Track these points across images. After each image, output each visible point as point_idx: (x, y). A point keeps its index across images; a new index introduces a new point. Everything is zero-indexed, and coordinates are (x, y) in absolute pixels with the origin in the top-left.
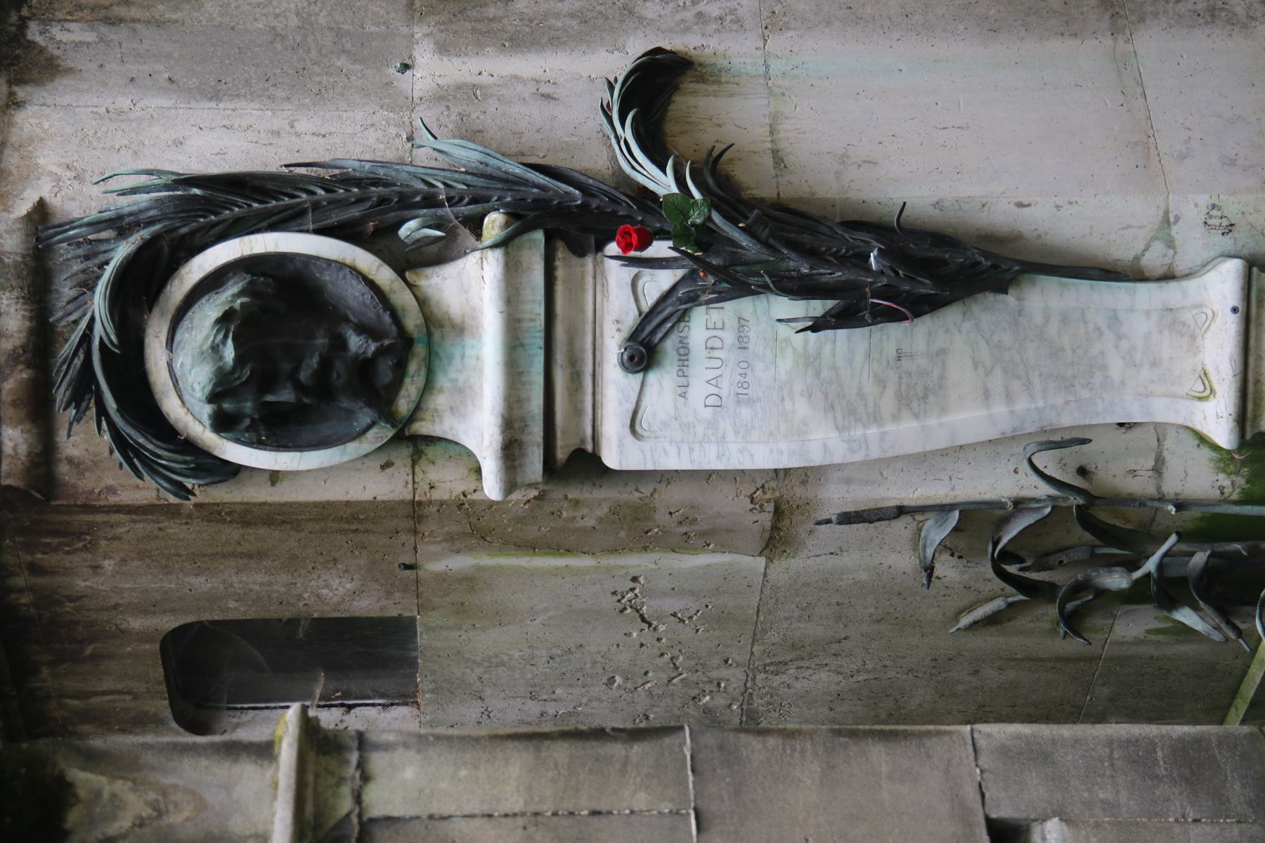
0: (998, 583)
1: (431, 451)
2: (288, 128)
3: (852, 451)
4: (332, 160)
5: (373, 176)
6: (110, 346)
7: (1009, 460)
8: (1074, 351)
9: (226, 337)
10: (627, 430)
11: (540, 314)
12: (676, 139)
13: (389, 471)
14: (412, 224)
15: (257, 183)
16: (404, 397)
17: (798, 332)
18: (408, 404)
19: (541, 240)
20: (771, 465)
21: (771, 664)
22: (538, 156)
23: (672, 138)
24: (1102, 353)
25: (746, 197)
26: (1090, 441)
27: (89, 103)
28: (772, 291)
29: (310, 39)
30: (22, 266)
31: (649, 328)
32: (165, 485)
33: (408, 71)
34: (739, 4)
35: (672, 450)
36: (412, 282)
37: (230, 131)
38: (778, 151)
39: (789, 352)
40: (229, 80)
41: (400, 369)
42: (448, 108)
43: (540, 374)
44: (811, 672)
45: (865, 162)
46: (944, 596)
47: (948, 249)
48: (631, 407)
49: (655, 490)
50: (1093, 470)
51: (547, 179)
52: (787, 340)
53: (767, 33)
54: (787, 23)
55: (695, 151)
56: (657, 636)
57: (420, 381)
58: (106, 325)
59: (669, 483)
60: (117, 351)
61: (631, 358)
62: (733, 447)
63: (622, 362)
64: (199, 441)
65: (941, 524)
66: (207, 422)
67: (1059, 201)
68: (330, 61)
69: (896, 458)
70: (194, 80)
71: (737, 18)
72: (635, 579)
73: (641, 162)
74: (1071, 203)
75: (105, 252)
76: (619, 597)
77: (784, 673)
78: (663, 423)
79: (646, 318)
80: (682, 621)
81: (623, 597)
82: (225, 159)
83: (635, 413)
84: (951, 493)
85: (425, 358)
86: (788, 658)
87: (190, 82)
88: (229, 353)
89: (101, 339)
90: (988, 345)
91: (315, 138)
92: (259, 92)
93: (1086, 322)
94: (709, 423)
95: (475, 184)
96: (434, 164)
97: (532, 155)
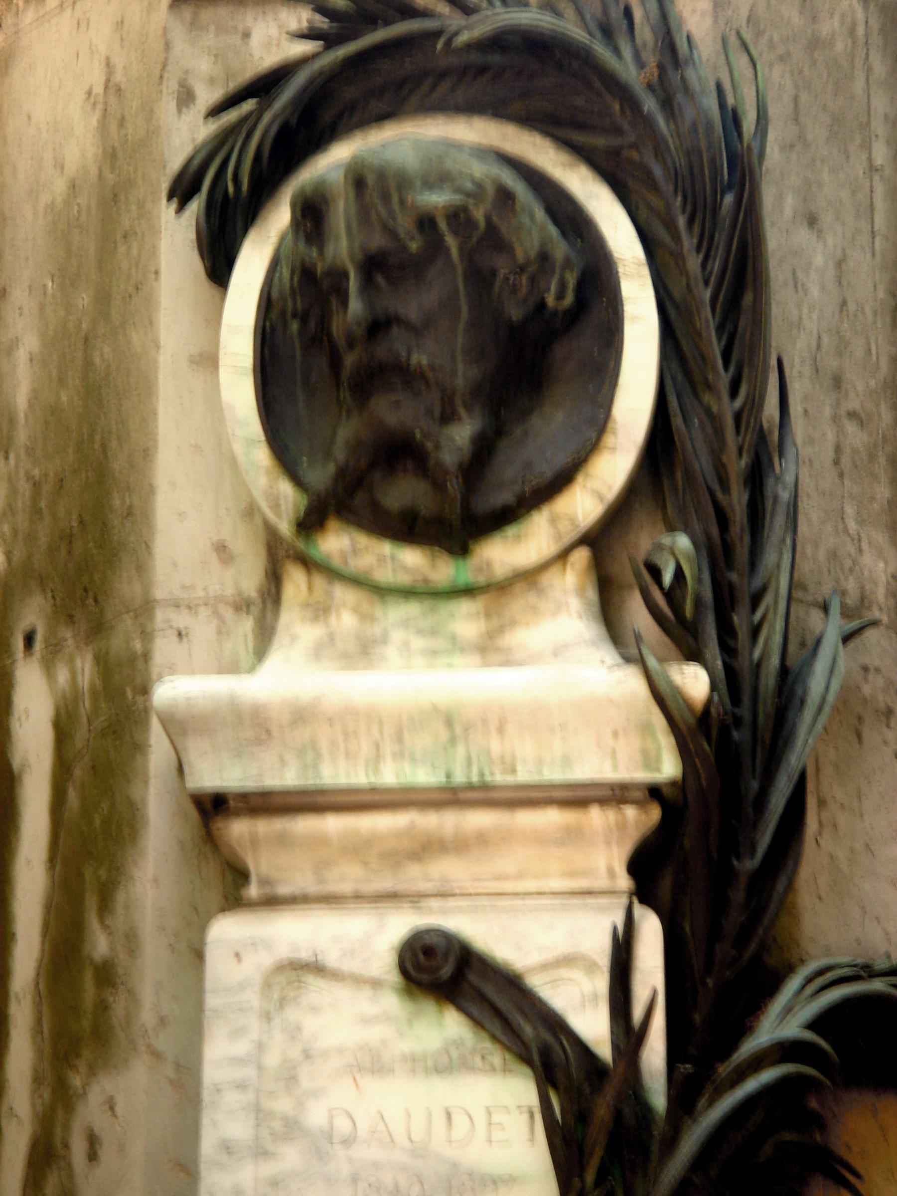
13: (214, 558)
15: (748, 299)
26: (92, 85)
31: (490, 991)
35: (242, 1047)
57: (385, 576)
97: (821, 824)
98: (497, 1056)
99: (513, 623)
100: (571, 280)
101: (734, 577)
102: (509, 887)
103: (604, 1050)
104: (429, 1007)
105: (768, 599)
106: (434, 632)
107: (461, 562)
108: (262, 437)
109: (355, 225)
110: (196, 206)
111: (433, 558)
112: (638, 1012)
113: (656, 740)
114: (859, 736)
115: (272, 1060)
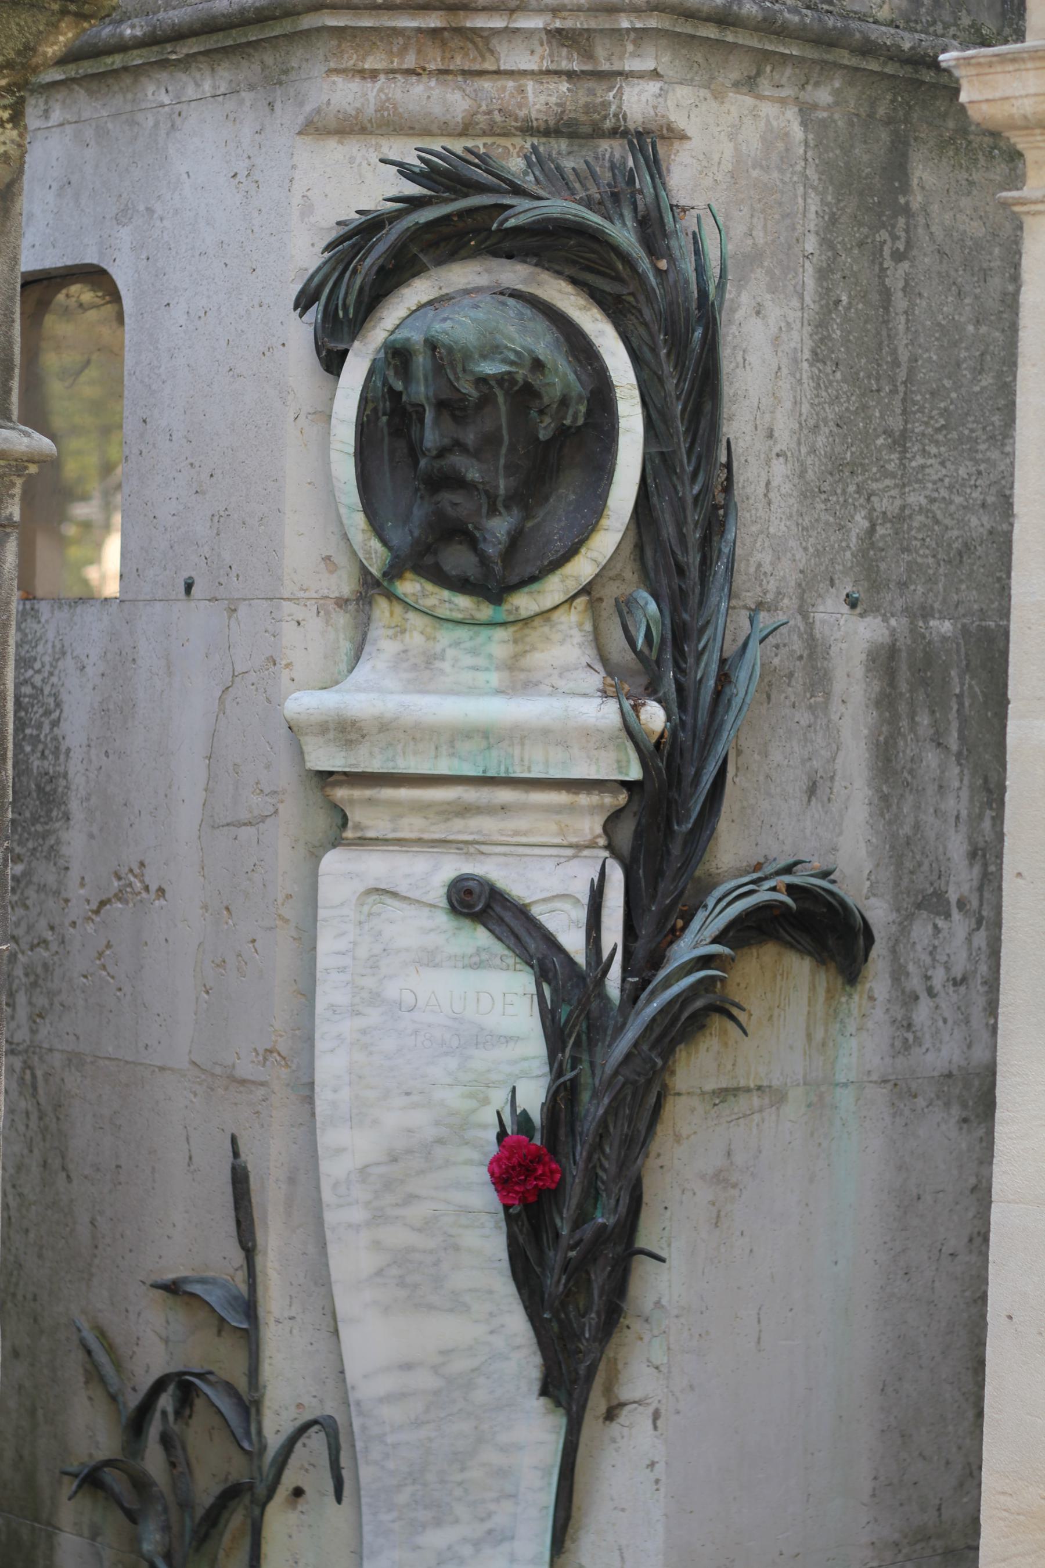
0: (146, 1383)
1: (342, 619)
2: (777, 449)
3: (336, 1185)
4: (735, 504)
5: (715, 558)
6: (501, 217)
7: (315, 1397)
8: (460, 1484)
9: (512, 363)
10: (372, 884)
11: (529, 771)
12: (754, 960)
14: (652, 607)
15: (708, 407)
16: (423, 588)
17: (498, 1113)
18: (414, 595)
19: (627, 775)
20: (319, 1077)
21: (34, 1076)
22: (736, 775)
23: (755, 954)
24: (457, 1521)
25: (677, 1049)
27: (809, 201)
28: (554, 1081)
29: (888, 482)
30: (603, 113)
31: (508, 916)
32: (316, 280)
33: (847, 607)
34: (927, 1050)
35: (342, 944)
36: (574, 604)
37: (773, 375)
38: (735, 1096)
39: (472, 1104)
40: (838, 375)
41: (462, 585)
42: (801, 658)
43: (450, 769)
44: (22, 1128)
45: (719, 1211)
46: (127, 1311)
47: (603, 1317)
48: (403, 890)
49: (287, 921)
50: (300, 1508)
51: (708, 786)
52: (485, 1101)
53: (889, 1086)
54: (901, 1114)
55: (738, 985)
56: (79, 922)
57: (443, 612)
58: (529, 214)
59: (295, 939)
60: (495, 226)
61: (469, 892)
62: (347, 1026)
63: (467, 879)
64: (372, 323)
65: (232, 1305)
66: (402, 334)
67: (660, 1467)
68: (862, 506)
69: (323, 1246)
70: (838, 332)
71: (910, 1047)
72: (161, 891)
73: (728, 910)
74: (657, 1481)
75: (622, 216)
76: (137, 871)
77: (21, 1093)
78: (380, 933)
79: (522, 912)
80: (100, 955)
81: (135, 876)
82: (737, 367)
83: (394, 895)
84: (272, 1319)
85: (473, 619)
86: (42, 1098)
87: (835, 327)
88: (490, 368)
89: (511, 207)
90: (473, 1370)
91: (763, 484)
92: (822, 414)
93: (497, 1500)
94: (378, 995)
95: (702, 691)
96: (728, 637)
97: (737, 769)
98: (511, 959)
99: (534, 648)
100: (583, 409)
101: (686, 616)
102: (524, 840)
103: (581, 959)
104: (467, 923)
105: (709, 633)
106: (474, 652)
107: (497, 608)
108: (352, 450)
109: (430, 378)
110: (314, 313)
111: (478, 603)
112: (605, 955)
113: (627, 754)
114: (769, 697)
115: (362, 952)
